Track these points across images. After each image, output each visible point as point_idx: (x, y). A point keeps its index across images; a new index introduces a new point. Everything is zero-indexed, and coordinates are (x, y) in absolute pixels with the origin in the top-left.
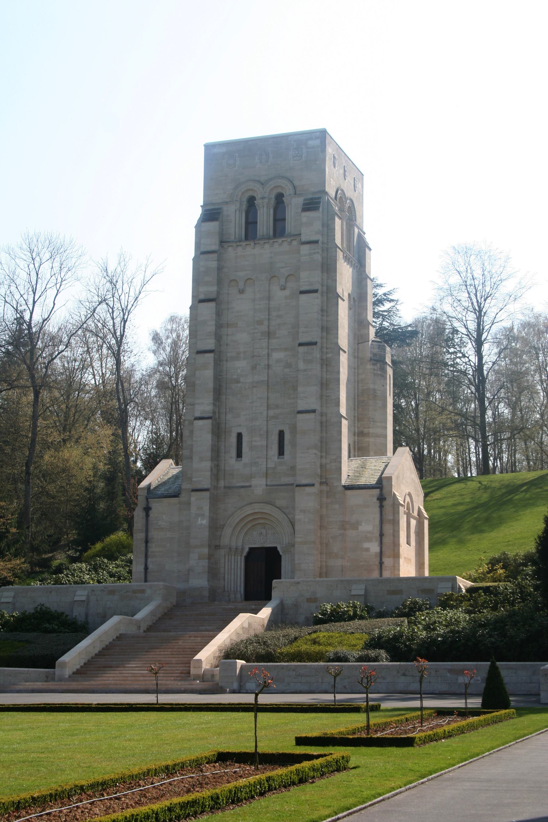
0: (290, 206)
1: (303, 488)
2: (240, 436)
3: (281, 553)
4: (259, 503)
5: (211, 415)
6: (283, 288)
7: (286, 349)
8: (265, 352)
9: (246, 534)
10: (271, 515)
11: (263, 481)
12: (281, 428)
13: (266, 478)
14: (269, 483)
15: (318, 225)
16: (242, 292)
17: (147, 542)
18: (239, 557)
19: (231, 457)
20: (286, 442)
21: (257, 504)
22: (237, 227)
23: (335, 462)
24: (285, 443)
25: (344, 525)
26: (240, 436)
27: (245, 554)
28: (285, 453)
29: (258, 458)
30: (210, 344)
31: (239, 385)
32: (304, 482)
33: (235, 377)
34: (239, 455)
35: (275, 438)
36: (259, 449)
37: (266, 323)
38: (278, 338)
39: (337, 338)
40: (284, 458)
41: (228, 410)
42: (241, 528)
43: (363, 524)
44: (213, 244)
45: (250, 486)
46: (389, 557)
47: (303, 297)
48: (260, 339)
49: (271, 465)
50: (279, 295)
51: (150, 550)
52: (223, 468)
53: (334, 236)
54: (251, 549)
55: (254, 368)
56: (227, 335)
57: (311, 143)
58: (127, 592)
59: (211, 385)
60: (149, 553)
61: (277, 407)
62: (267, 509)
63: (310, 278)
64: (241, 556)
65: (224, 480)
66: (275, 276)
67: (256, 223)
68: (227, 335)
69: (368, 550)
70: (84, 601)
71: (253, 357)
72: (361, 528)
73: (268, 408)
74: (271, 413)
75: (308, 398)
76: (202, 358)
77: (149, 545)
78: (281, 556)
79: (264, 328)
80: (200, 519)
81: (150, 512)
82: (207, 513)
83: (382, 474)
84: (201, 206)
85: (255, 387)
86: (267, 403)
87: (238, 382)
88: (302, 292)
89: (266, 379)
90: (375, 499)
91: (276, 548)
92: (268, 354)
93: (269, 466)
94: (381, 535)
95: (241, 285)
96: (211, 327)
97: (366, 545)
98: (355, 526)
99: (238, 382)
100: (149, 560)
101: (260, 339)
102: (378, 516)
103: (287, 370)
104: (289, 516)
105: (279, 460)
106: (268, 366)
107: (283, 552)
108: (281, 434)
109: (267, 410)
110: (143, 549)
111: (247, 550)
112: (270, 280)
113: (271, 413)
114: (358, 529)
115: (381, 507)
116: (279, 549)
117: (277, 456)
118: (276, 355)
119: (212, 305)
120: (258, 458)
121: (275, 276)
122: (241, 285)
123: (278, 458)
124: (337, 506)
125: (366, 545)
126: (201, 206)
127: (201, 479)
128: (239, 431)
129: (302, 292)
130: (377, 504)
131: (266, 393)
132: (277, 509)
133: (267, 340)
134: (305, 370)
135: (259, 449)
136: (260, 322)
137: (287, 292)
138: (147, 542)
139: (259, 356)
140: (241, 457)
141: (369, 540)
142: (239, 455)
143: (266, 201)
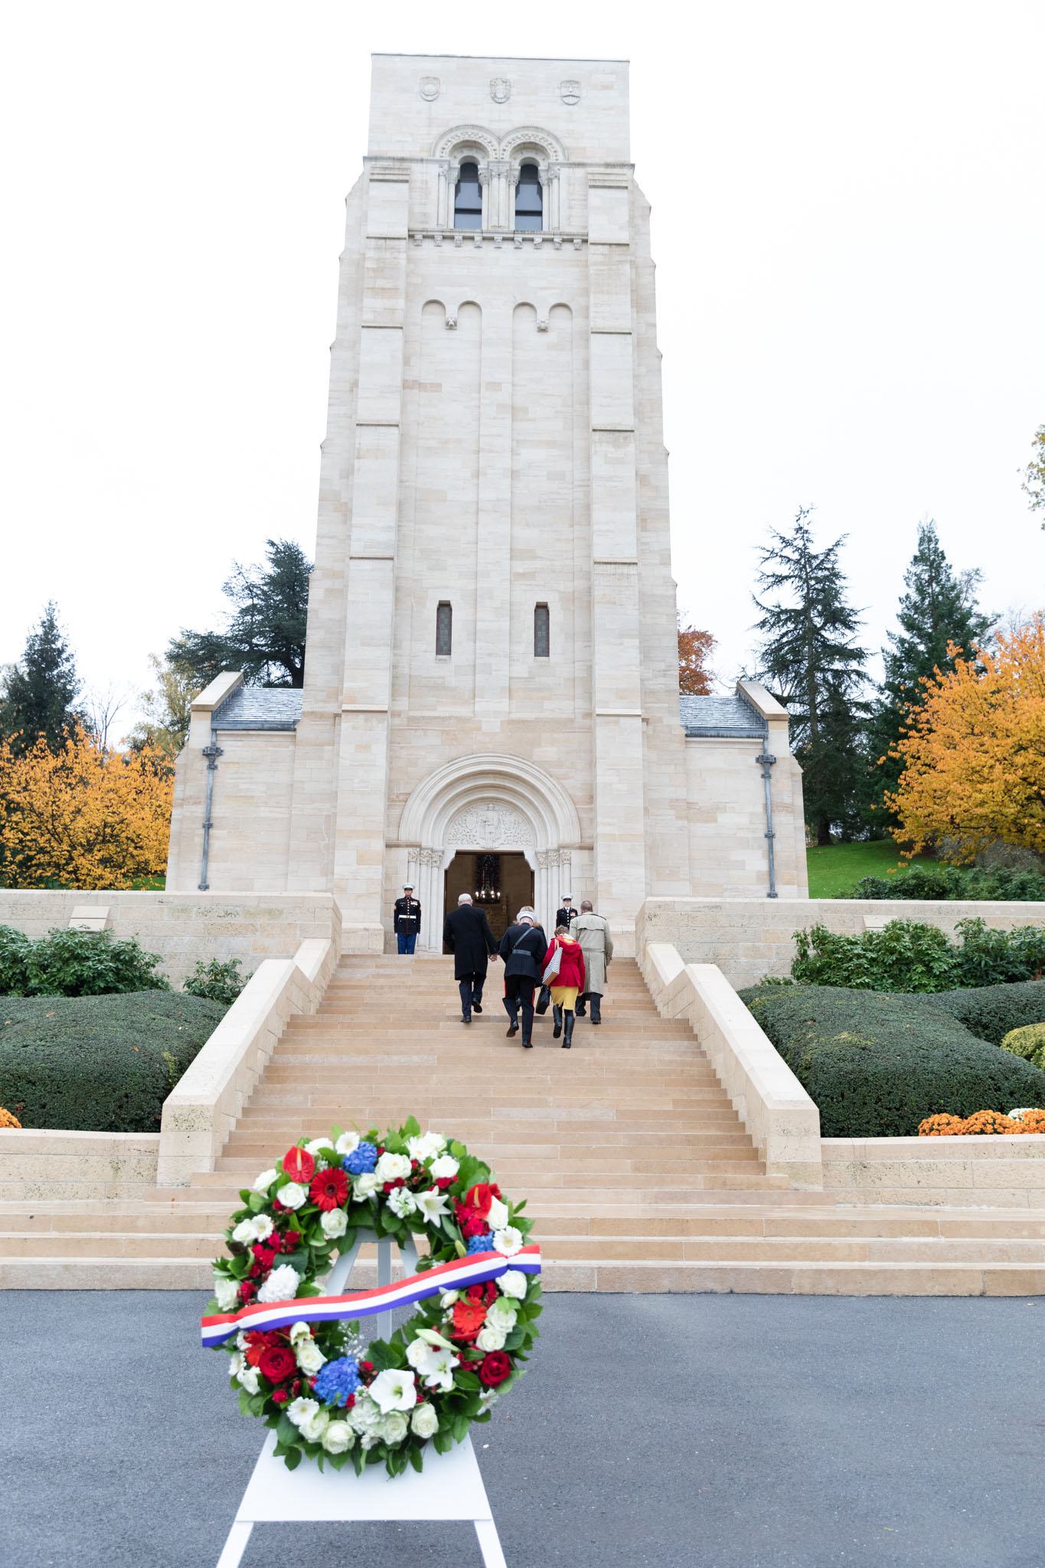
0: (555, 181)
3: (533, 866)
9: (458, 811)
17: (208, 826)
22: (441, 205)
23: (665, 676)
27: (446, 865)
29: (490, 655)
39: (661, 432)
42: (457, 795)
46: (788, 883)
54: (458, 853)
58: (228, 914)
69: (741, 865)
74: (520, 567)
75: (615, 535)
76: (367, 438)
91: (521, 854)
95: (452, 311)
110: (199, 840)
111: (450, 856)
116: (529, 857)
138: (208, 826)
139: (491, 452)
140: (449, 652)
142: (444, 646)
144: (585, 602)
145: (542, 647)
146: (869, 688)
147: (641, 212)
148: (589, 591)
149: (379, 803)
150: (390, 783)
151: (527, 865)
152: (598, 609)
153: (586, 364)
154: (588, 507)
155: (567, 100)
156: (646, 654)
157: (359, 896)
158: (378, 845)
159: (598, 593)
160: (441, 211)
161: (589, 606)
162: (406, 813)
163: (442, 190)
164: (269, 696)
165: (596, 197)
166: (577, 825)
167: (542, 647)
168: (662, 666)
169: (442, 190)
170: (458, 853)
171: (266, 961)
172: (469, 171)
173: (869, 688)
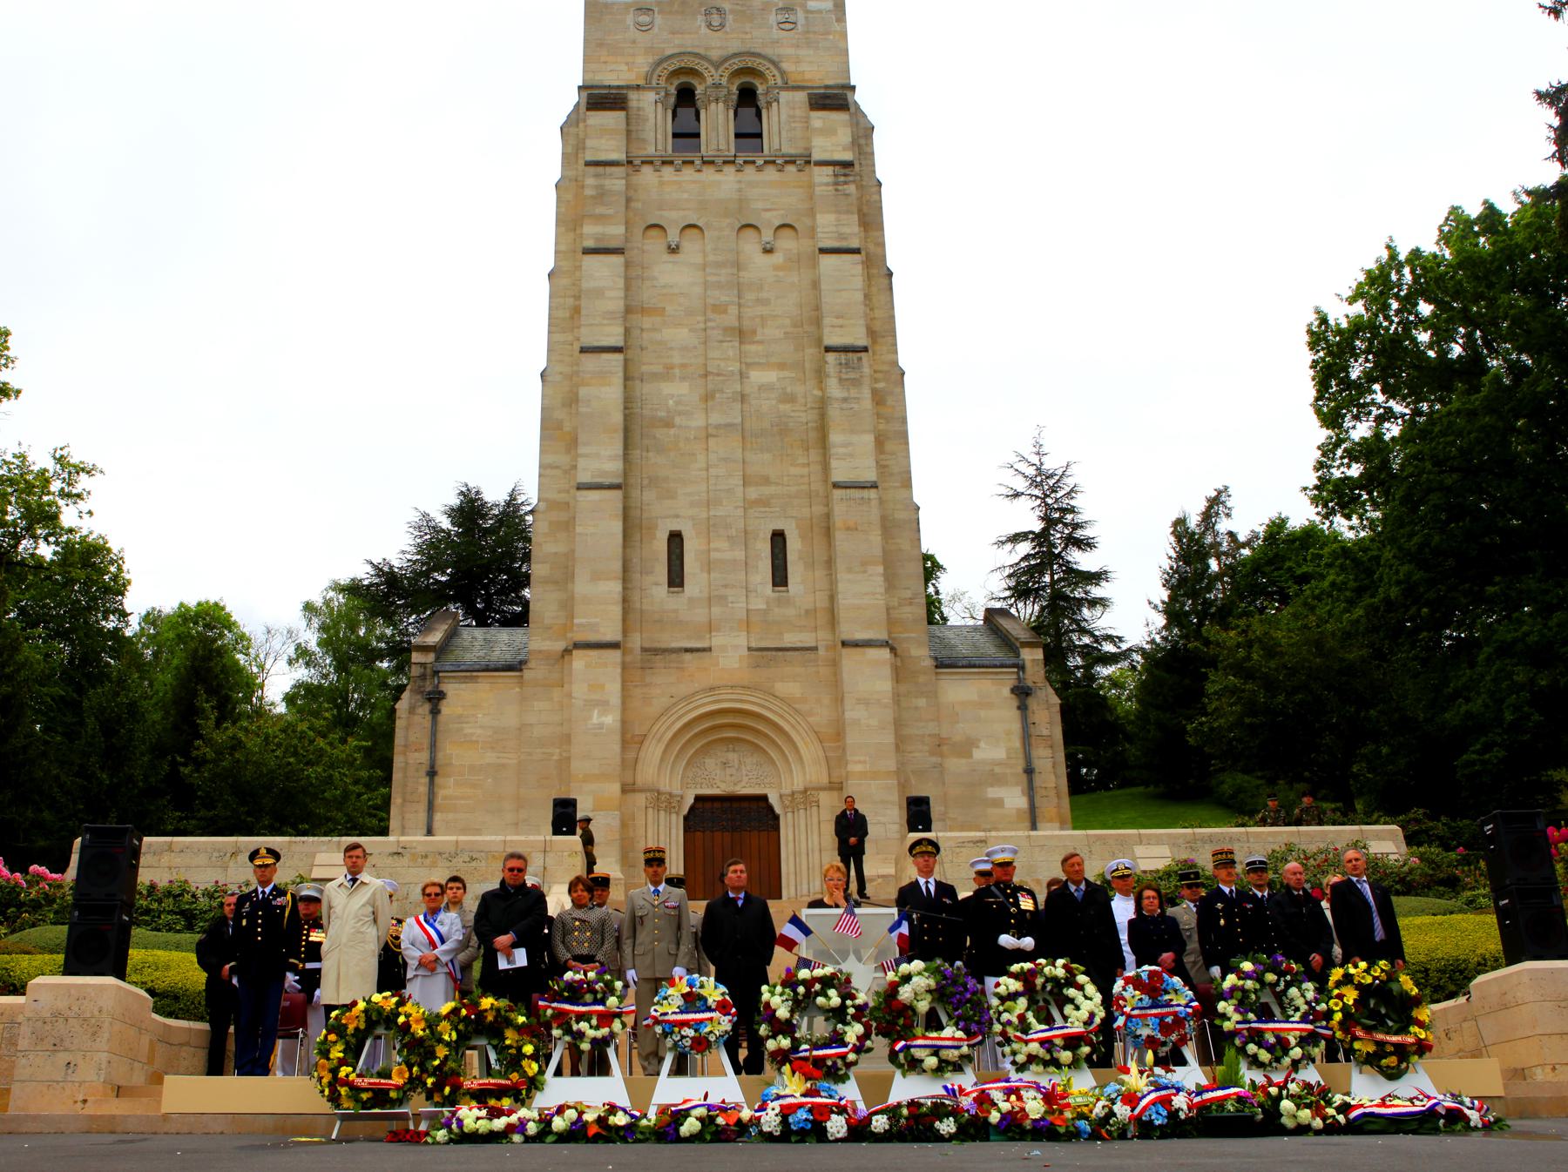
2: (676, 539)
3: (778, 810)
4: (995, 666)
5: (619, 480)
7: (782, 366)
8: (734, 367)
11: (742, 640)
14: (753, 645)
17: (432, 773)
19: (657, 584)
20: (792, 556)
25: (939, 745)
26: (676, 539)
27: (685, 811)
29: (725, 586)
31: (672, 431)
32: (860, 636)
33: (662, 414)
34: (676, 578)
36: (727, 574)
37: (733, 310)
38: (761, 342)
43: (982, 744)
45: (709, 649)
47: (828, 261)
51: (441, 793)
52: (638, 605)
55: (708, 397)
59: (617, 418)
60: (439, 801)
61: (766, 481)
63: (831, 225)
69: (998, 803)
72: (978, 754)
73: (746, 482)
74: (753, 493)
76: (591, 362)
77: (438, 780)
78: (777, 818)
83: (1156, 607)
87: (668, 424)
88: (823, 251)
89: (739, 420)
91: (764, 798)
94: (1029, 771)
95: (673, 236)
97: (993, 792)
98: (966, 748)
99: (668, 424)
100: (438, 817)
102: (1016, 726)
103: (785, 408)
107: (785, 807)
108: (778, 538)
113: (753, 493)
114: (971, 756)
116: (774, 800)
118: (757, 377)
122: (673, 236)
125: (993, 792)
126: (182, 605)
128: (675, 527)
134: (845, 400)
135: (727, 574)
140: (681, 585)
141: (999, 780)
142: (676, 578)
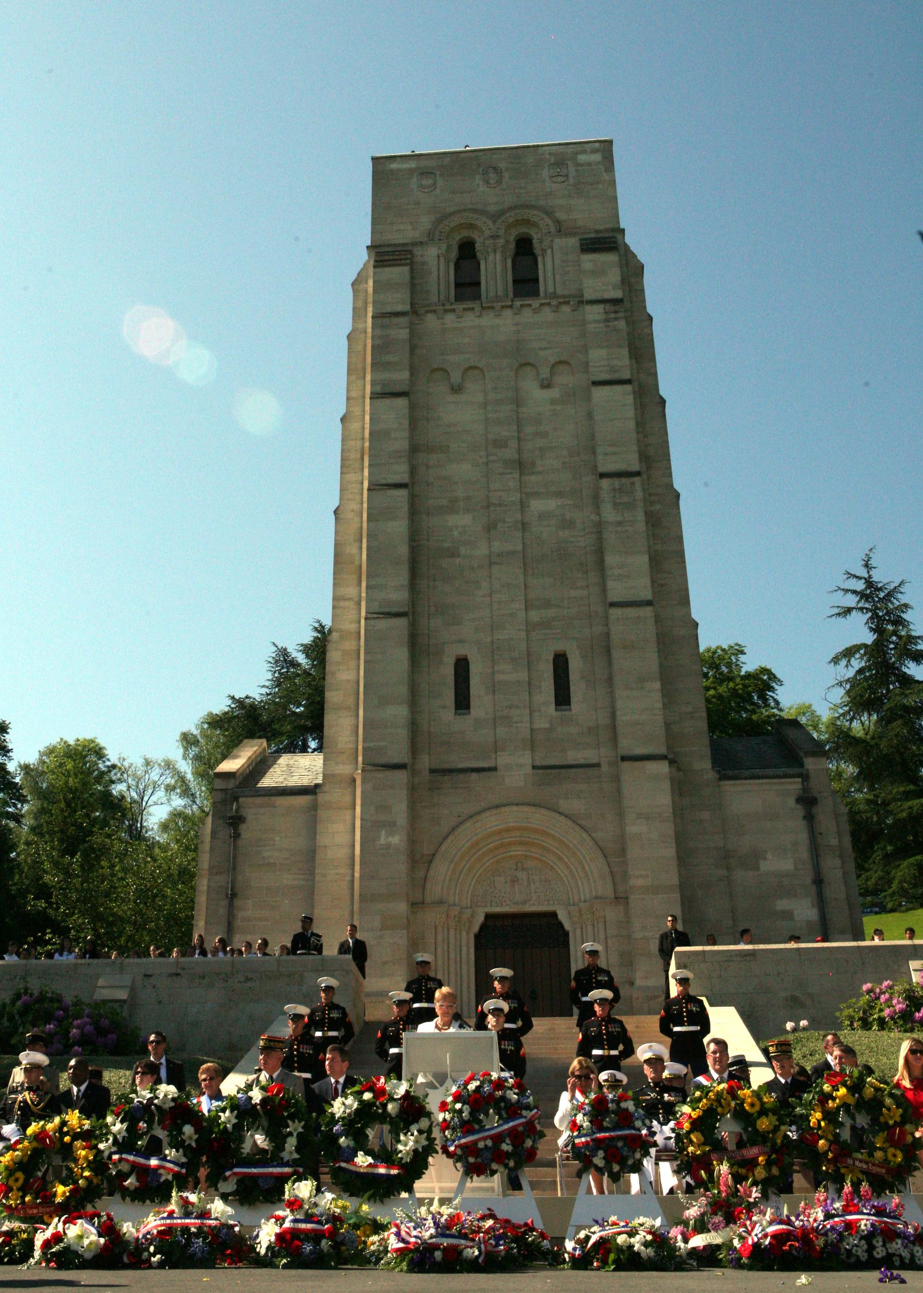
1: (638, 764)
3: (567, 926)
6: (546, 385)
7: (560, 494)
8: (516, 497)
10: (548, 835)
11: (526, 759)
12: (560, 647)
13: (533, 751)
15: (615, 276)
16: (457, 389)
18: (464, 934)
19: (444, 707)
21: (515, 808)
24: (572, 677)
25: (726, 857)
26: (462, 667)
27: (476, 928)
28: (574, 700)
30: (399, 472)
31: (457, 561)
35: (546, 670)
37: (513, 444)
38: (540, 473)
40: (570, 710)
41: (433, 609)
43: (769, 856)
44: (399, 301)
45: (494, 769)
48: (502, 474)
49: (542, 724)
50: (538, 398)
51: (240, 915)
53: (644, 301)
55: (490, 527)
56: (428, 467)
57: (582, 158)
60: (238, 923)
61: (547, 604)
62: (538, 818)
64: (468, 933)
65: (429, 754)
66: (528, 364)
67: (478, 284)
68: (428, 467)
70: (124, 1001)
71: (488, 507)
72: (765, 866)
74: (534, 616)
77: (238, 902)
78: (566, 934)
79: (510, 453)
80: (383, 832)
81: (243, 828)
82: (402, 819)
84: (367, 247)
85: (495, 563)
86: (526, 596)
88: (596, 383)
90: (791, 802)
91: (554, 915)
92: (522, 502)
93: (536, 726)
94: (819, 881)
95: (456, 377)
96: (400, 443)
97: (782, 904)
98: (752, 859)
101: (502, 474)
103: (564, 534)
104: (593, 835)
105: (559, 713)
106: (524, 526)
109: (526, 609)
111: (481, 919)
112: (517, 370)
114: (758, 868)
115: (809, 818)
116: (562, 916)
117: (553, 706)
118: (537, 505)
119: (402, 402)
120: (510, 707)
121: (528, 364)
123: (556, 710)
124: (705, 815)
125: (782, 904)
127: (383, 744)
129: (596, 383)
130: (800, 811)
131: (522, 576)
132: (562, 818)
133: (517, 476)
134: (620, 523)
136: (500, 444)
137: (554, 393)
139: (500, 505)
140: (468, 707)
142: (462, 702)
143: (501, 241)
144: (604, 647)
145: (562, 697)
146: (267, 781)
147: (632, 271)
148: (607, 635)
149: (402, 867)
150: (413, 842)
151: (560, 925)
152: (616, 654)
153: (590, 416)
154: (600, 553)
155: (554, 179)
156: (669, 695)
157: (385, 963)
158: (402, 907)
159: (615, 638)
160: (442, 287)
161: (608, 651)
162: (432, 873)
163: (442, 266)
164: (291, 762)
165: (589, 261)
166: (609, 879)
167: (562, 697)
168: (690, 709)
169: (442, 266)
170: (488, 916)
171: (661, 393)
172: (467, 252)
173: (267, 781)
